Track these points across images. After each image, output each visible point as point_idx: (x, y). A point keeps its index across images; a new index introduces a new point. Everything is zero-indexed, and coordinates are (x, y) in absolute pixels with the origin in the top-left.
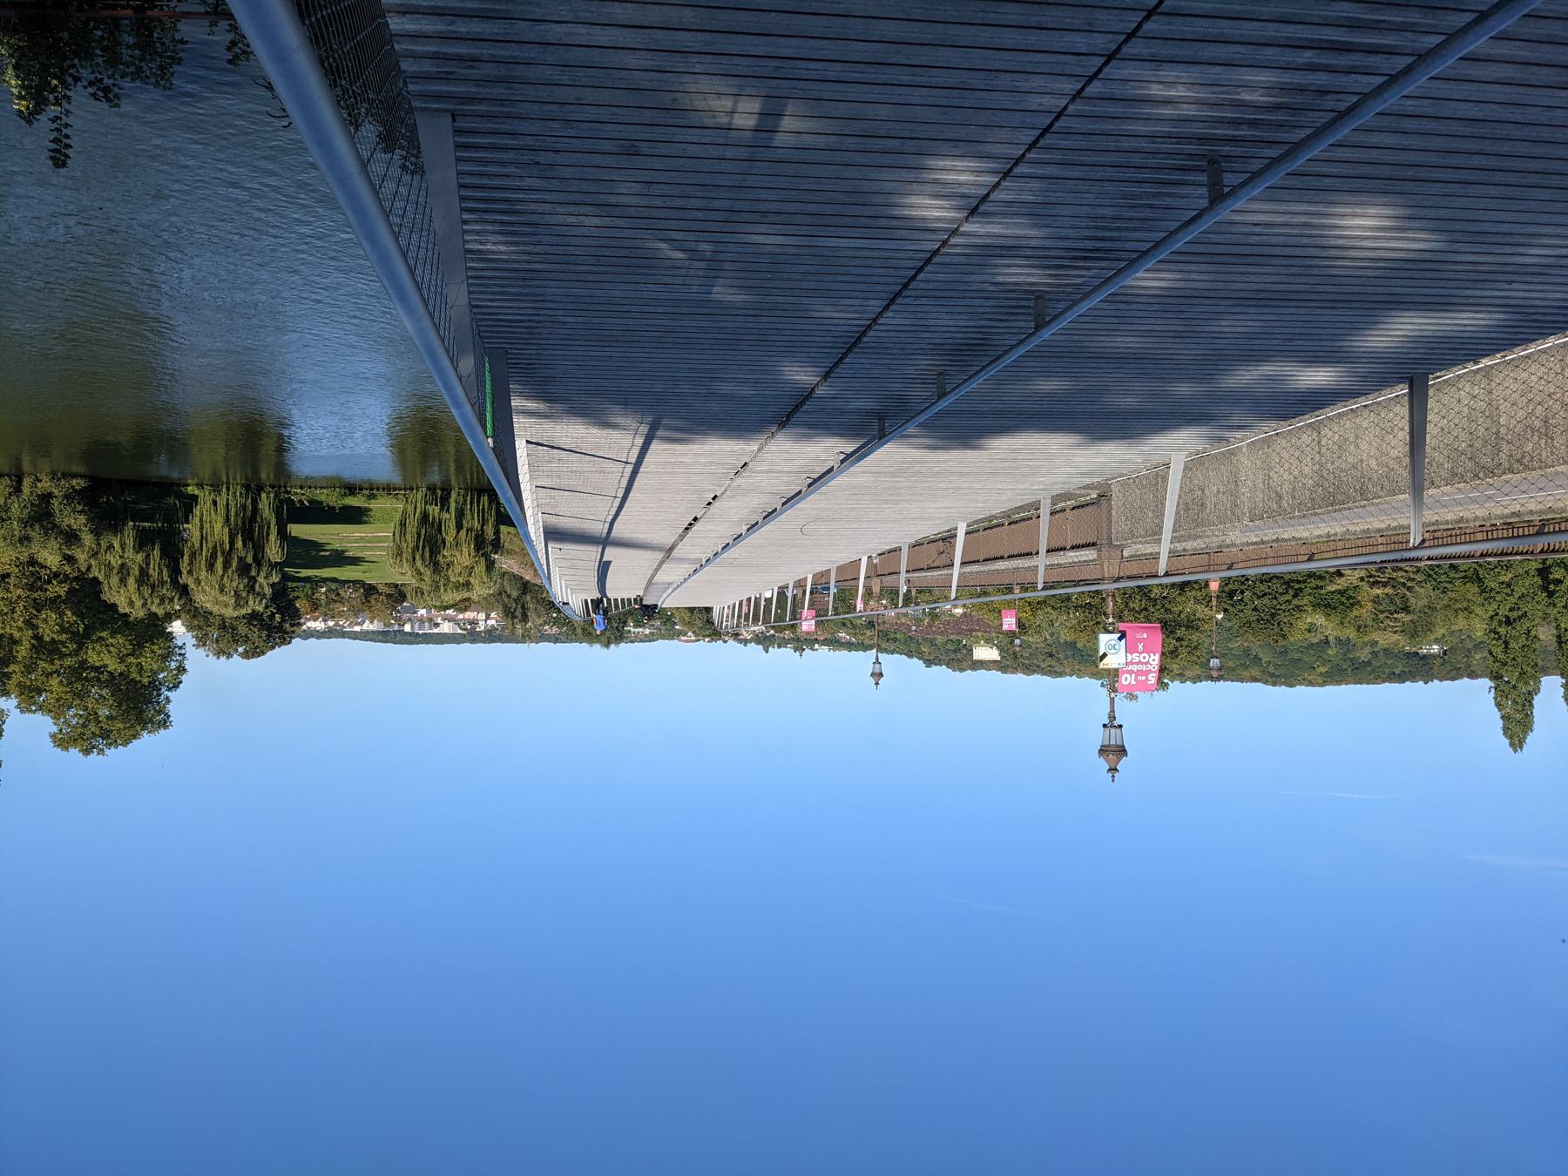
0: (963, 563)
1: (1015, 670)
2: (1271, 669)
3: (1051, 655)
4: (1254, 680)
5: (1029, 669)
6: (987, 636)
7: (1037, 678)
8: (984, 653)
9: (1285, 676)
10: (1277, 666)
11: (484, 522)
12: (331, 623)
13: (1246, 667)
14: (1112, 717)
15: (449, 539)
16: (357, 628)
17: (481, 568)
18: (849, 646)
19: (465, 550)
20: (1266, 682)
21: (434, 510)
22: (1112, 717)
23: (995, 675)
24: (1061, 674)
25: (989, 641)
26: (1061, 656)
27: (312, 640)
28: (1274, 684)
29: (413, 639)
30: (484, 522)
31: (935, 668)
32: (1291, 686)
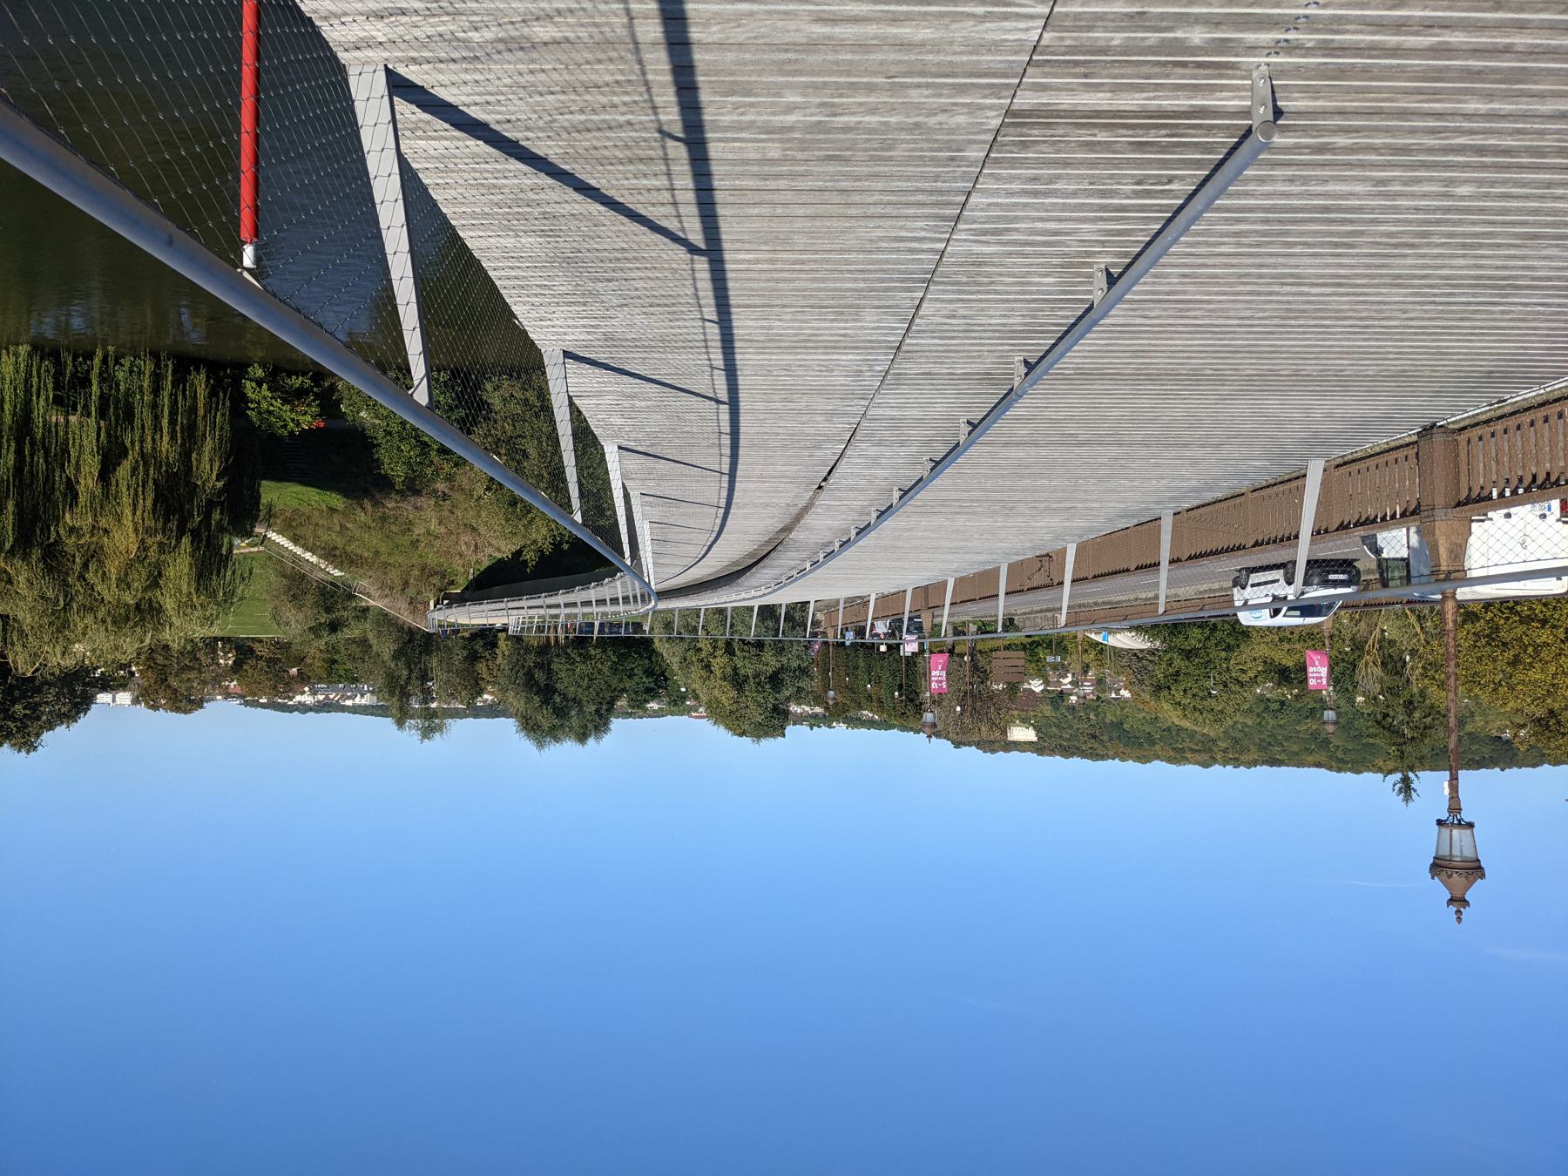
0: (1172, 562)
1: (1052, 752)
2: (1340, 754)
3: (1094, 737)
4: (1319, 765)
5: (1067, 751)
6: (1023, 714)
7: (1076, 762)
8: (1022, 733)
9: (1353, 762)
10: (1346, 751)
11: (190, 438)
12: (321, 698)
13: (1310, 752)
14: (1455, 808)
15: (88, 483)
16: (349, 703)
17: (180, 567)
18: (871, 724)
19: (128, 521)
20: (1331, 768)
21: (973, 628)
22: (1455, 808)
23: (1031, 757)
24: (1102, 757)
25: (1025, 721)
26: (1105, 738)
27: (311, 714)
28: (1339, 770)
29: (290, 709)
30: (190, 438)
31: (965, 749)
32: (1358, 772)
